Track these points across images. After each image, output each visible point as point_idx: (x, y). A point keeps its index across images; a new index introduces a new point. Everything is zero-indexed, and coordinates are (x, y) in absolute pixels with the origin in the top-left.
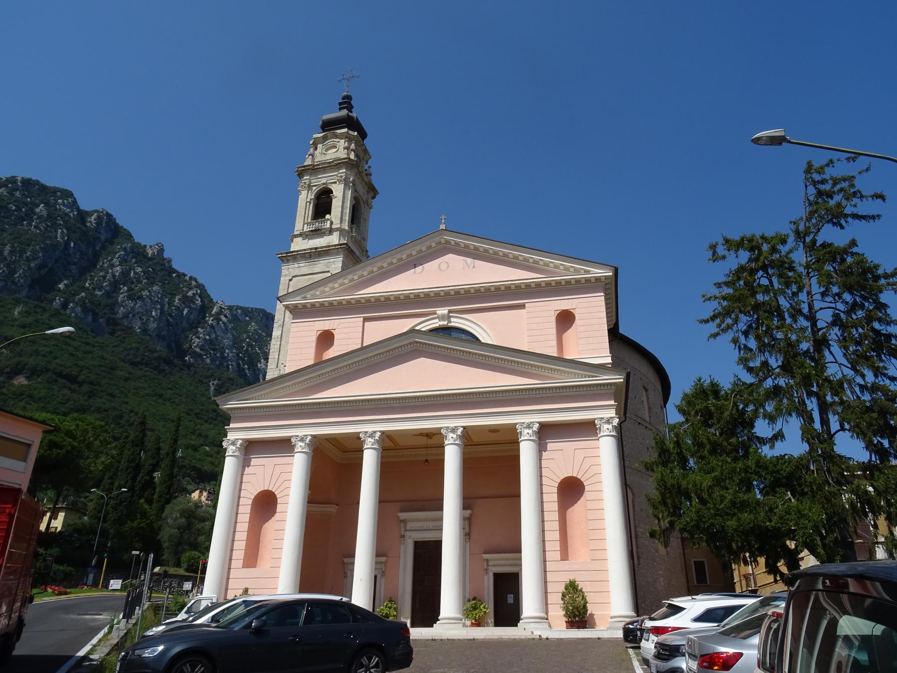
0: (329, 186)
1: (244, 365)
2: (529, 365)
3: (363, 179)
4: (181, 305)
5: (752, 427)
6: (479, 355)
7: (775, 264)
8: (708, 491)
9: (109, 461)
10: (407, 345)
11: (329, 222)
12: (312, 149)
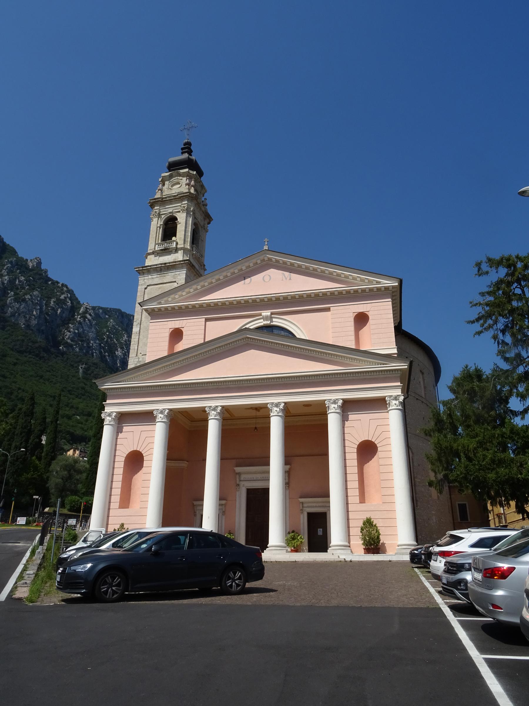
0: (174, 215)
1: (105, 352)
2: (334, 355)
3: (201, 209)
4: (56, 306)
5: (507, 403)
6: (296, 347)
7: (527, 278)
8: (473, 451)
9: (8, 427)
10: (241, 340)
11: (175, 243)
12: (161, 185)
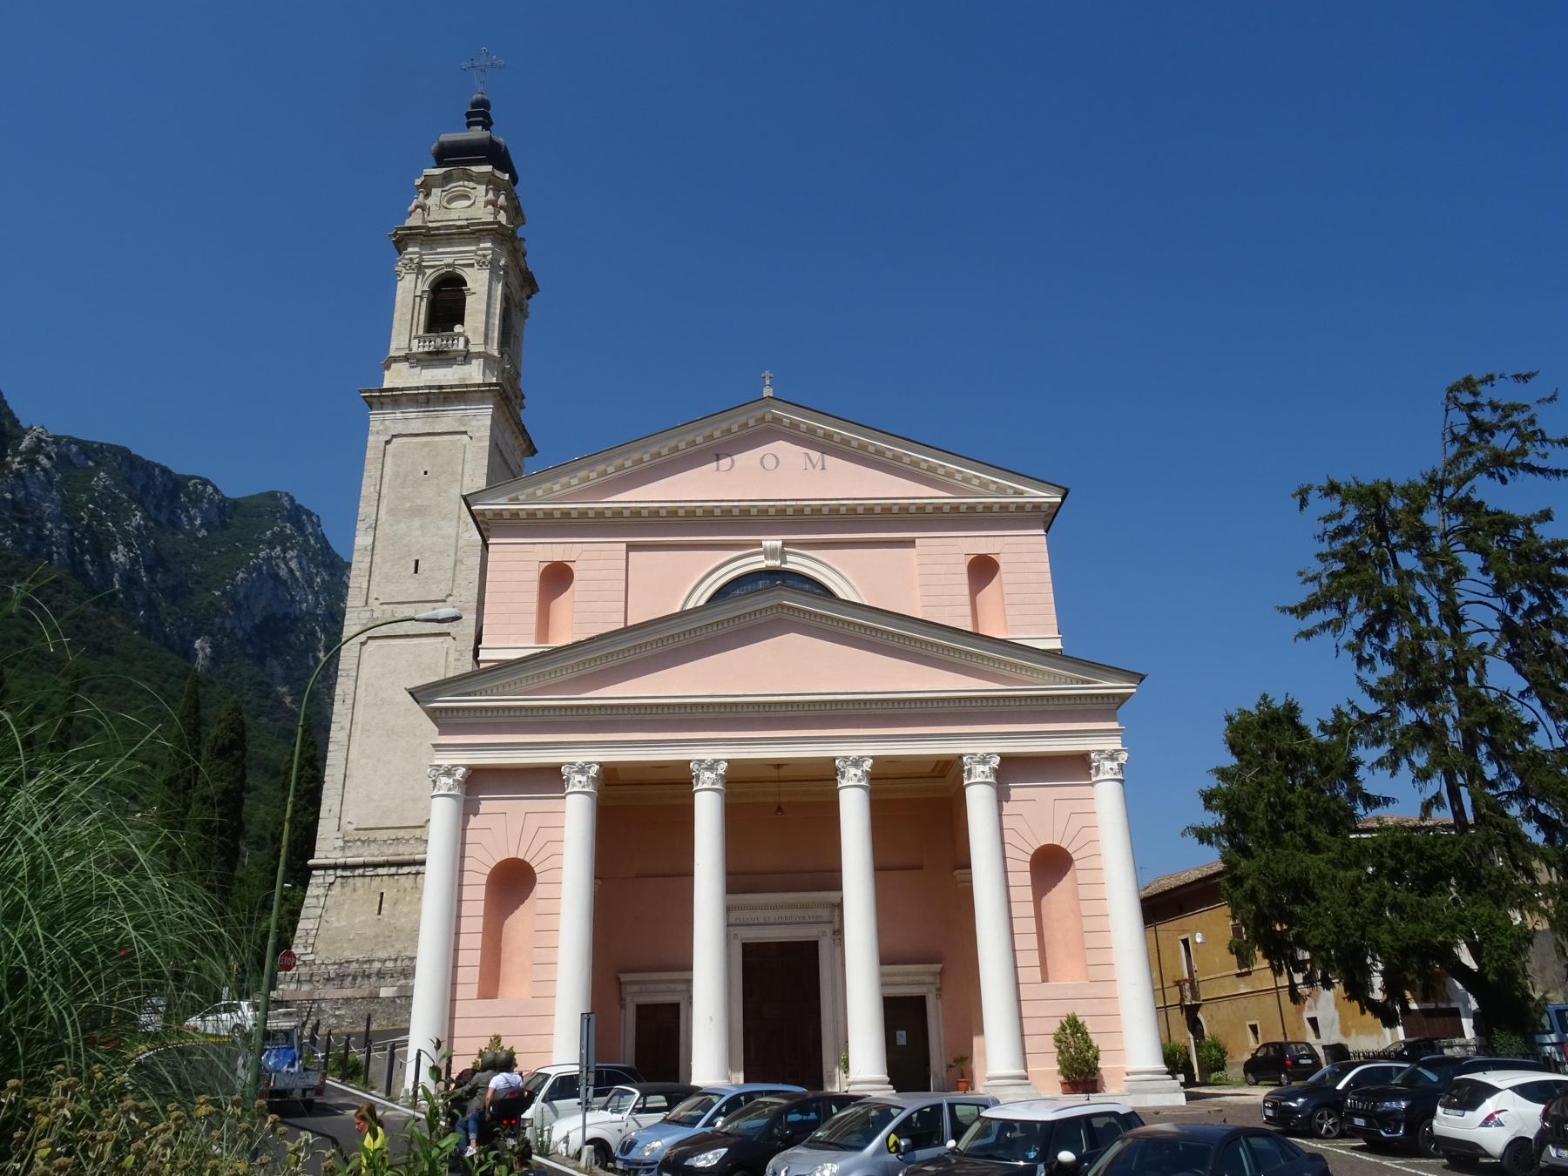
0: (458, 271)
1: (83, 553)
11: (462, 340)
